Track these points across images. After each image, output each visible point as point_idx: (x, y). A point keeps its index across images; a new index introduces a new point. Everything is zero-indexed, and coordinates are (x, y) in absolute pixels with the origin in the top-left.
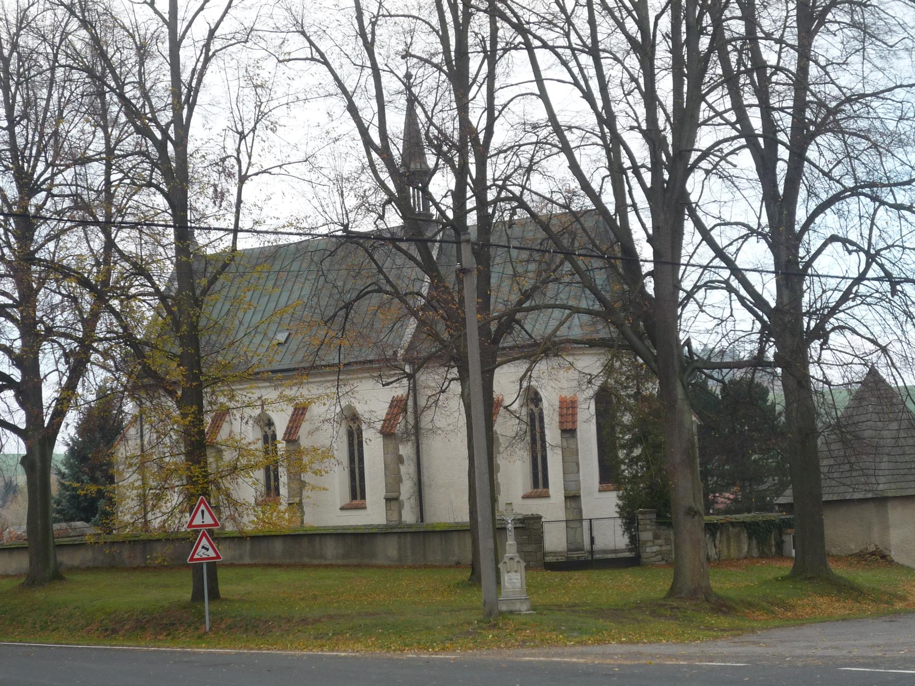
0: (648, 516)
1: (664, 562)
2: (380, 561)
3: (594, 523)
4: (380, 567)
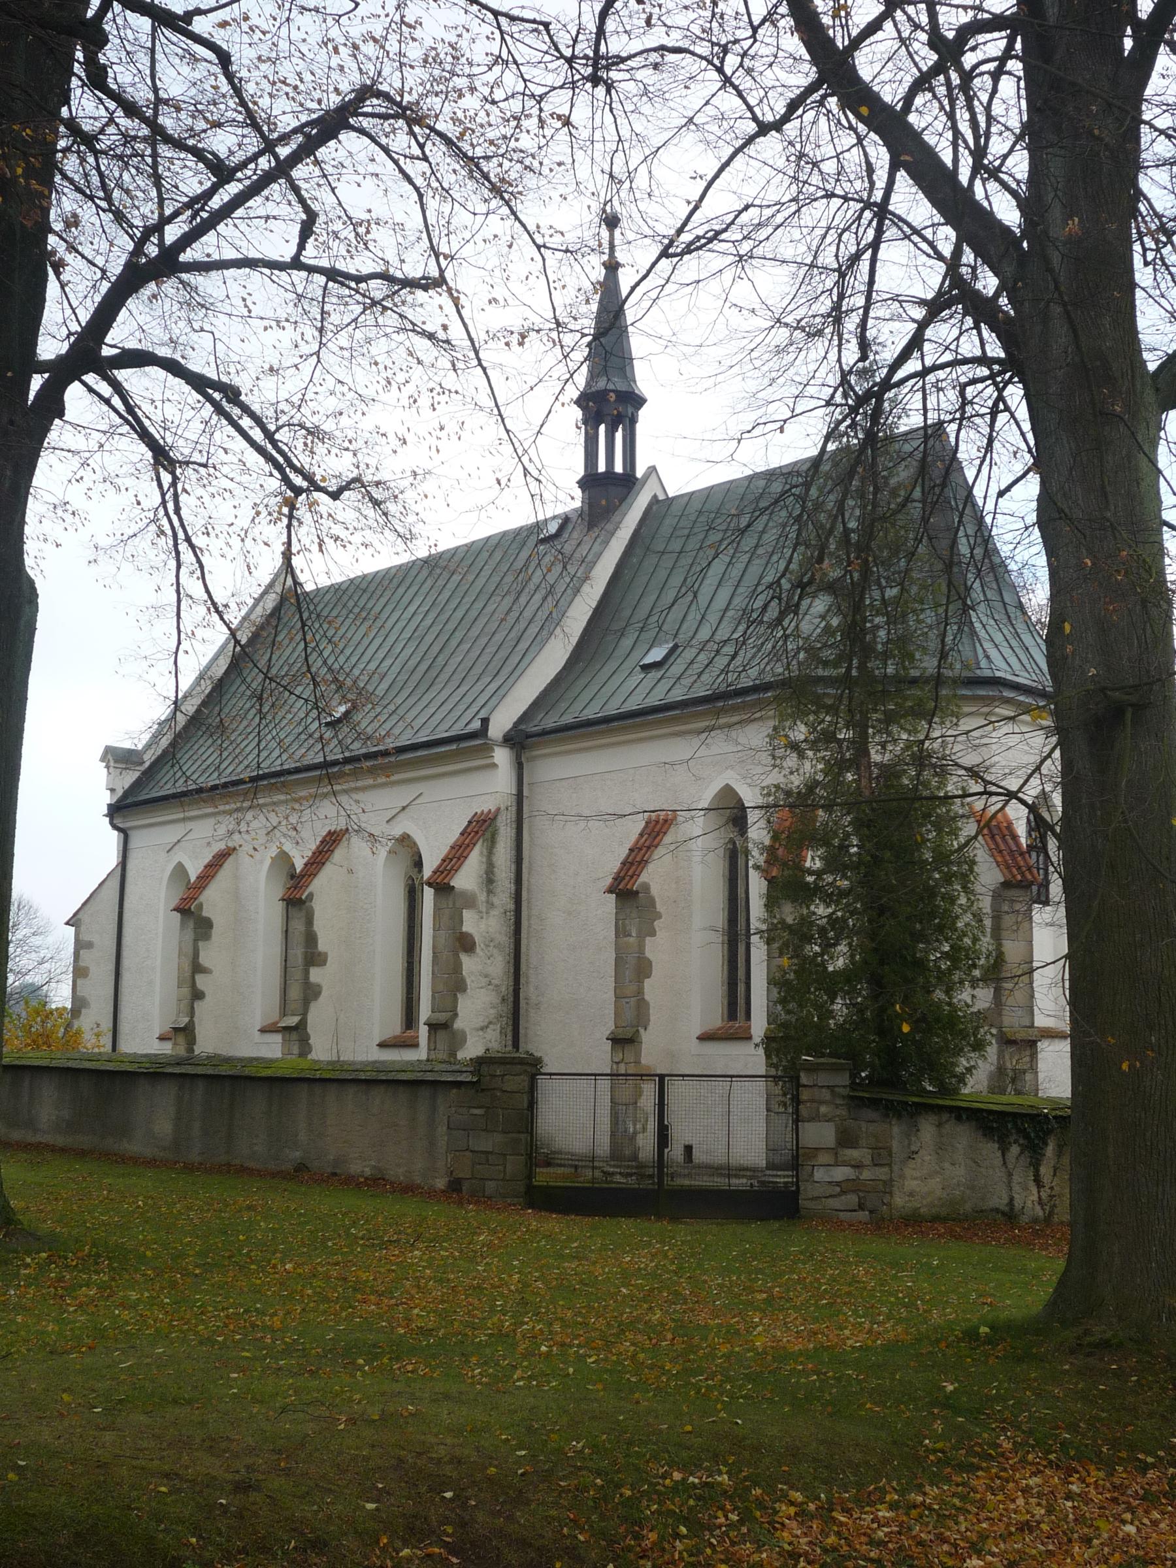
0: (823, 1078)
1: (863, 1215)
2: (134, 1147)
3: (677, 1091)
4: (136, 1161)
